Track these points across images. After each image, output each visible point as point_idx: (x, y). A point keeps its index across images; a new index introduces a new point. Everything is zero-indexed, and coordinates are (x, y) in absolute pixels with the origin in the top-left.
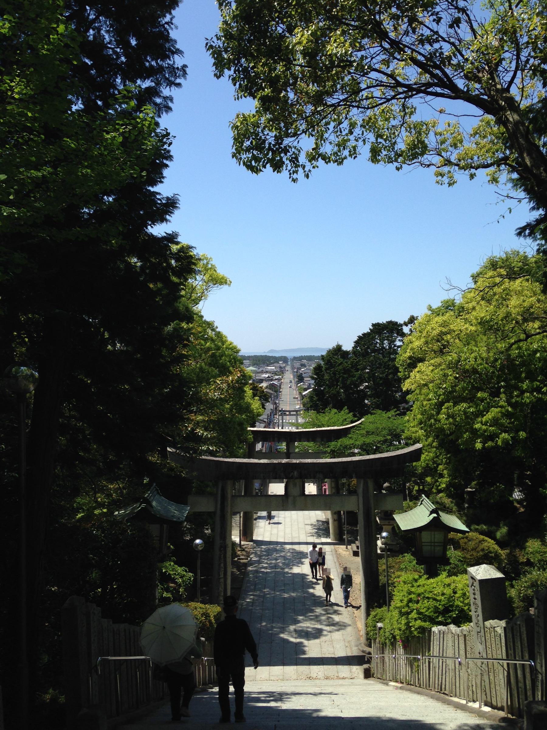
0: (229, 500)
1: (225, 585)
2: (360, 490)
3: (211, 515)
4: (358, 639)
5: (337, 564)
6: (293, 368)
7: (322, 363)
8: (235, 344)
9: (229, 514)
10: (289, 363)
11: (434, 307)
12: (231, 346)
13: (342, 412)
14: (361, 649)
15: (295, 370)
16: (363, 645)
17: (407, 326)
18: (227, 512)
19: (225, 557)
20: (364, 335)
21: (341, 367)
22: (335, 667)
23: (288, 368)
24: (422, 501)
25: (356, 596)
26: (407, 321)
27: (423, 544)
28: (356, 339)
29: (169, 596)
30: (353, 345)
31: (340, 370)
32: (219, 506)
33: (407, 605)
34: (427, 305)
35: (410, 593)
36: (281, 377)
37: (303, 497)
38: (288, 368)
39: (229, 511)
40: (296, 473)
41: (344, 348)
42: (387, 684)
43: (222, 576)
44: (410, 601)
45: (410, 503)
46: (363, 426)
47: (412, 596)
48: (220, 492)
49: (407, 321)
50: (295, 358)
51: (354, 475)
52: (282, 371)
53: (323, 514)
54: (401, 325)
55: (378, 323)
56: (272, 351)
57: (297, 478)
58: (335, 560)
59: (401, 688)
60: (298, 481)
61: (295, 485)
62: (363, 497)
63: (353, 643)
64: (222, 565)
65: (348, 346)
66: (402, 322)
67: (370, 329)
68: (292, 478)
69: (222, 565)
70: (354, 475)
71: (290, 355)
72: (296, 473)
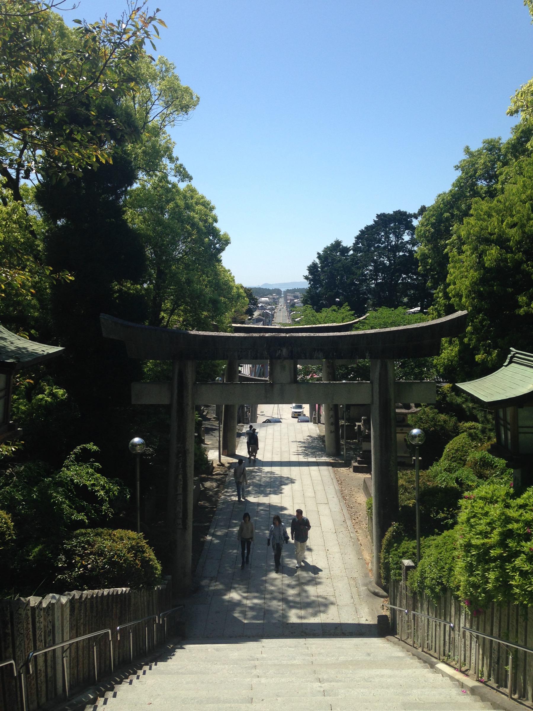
0: (190, 387)
1: (185, 504)
2: (376, 374)
3: (168, 408)
4: (366, 576)
5: (335, 481)
6: (286, 300)
7: (317, 261)
8: (208, 198)
9: (189, 408)
10: (283, 295)
11: (474, 149)
12: (202, 201)
13: (342, 310)
14: (372, 589)
15: (289, 301)
16: (374, 584)
17: (417, 218)
18: (188, 404)
19: (184, 467)
20: (367, 228)
21: (339, 264)
22: (342, 622)
23: (282, 301)
24: (512, 358)
25: (360, 518)
26: (416, 212)
27: (521, 430)
28: (358, 233)
29: (81, 518)
30: (353, 241)
31: (340, 267)
32: (175, 396)
33: (502, 544)
34: (463, 147)
35: (508, 520)
36: (274, 307)
37: (294, 386)
38: (282, 301)
39: (190, 403)
40: (284, 350)
41: (344, 244)
42: (432, 666)
43: (180, 491)
44: (508, 534)
45: (426, 409)
46: (367, 321)
47: (514, 526)
48: (176, 377)
49: (416, 212)
50: (288, 291)
51: (367, 354)
52: (275, 302)
53: (317, 428)
54: (411, 216)
55: (384, 213)
56: (266, 284)
57: (285, 358)
58: (332, 477)
59: (473, 691)
60: (287, 363)
61: (283, 368)
62: (380, 384)
63: (360, 582)
64: (180, 477)
65: (348, 242)
66: (412, 212)
67: (375, 221)
68: (279, 358)
69: (180, 477)
70: (367, 354)
71: (283, 290)
72: (284, 350)
